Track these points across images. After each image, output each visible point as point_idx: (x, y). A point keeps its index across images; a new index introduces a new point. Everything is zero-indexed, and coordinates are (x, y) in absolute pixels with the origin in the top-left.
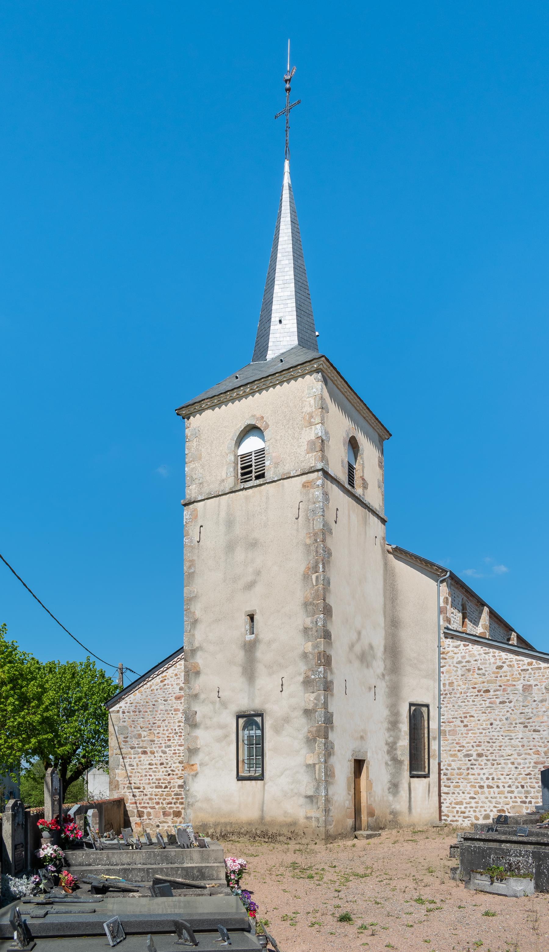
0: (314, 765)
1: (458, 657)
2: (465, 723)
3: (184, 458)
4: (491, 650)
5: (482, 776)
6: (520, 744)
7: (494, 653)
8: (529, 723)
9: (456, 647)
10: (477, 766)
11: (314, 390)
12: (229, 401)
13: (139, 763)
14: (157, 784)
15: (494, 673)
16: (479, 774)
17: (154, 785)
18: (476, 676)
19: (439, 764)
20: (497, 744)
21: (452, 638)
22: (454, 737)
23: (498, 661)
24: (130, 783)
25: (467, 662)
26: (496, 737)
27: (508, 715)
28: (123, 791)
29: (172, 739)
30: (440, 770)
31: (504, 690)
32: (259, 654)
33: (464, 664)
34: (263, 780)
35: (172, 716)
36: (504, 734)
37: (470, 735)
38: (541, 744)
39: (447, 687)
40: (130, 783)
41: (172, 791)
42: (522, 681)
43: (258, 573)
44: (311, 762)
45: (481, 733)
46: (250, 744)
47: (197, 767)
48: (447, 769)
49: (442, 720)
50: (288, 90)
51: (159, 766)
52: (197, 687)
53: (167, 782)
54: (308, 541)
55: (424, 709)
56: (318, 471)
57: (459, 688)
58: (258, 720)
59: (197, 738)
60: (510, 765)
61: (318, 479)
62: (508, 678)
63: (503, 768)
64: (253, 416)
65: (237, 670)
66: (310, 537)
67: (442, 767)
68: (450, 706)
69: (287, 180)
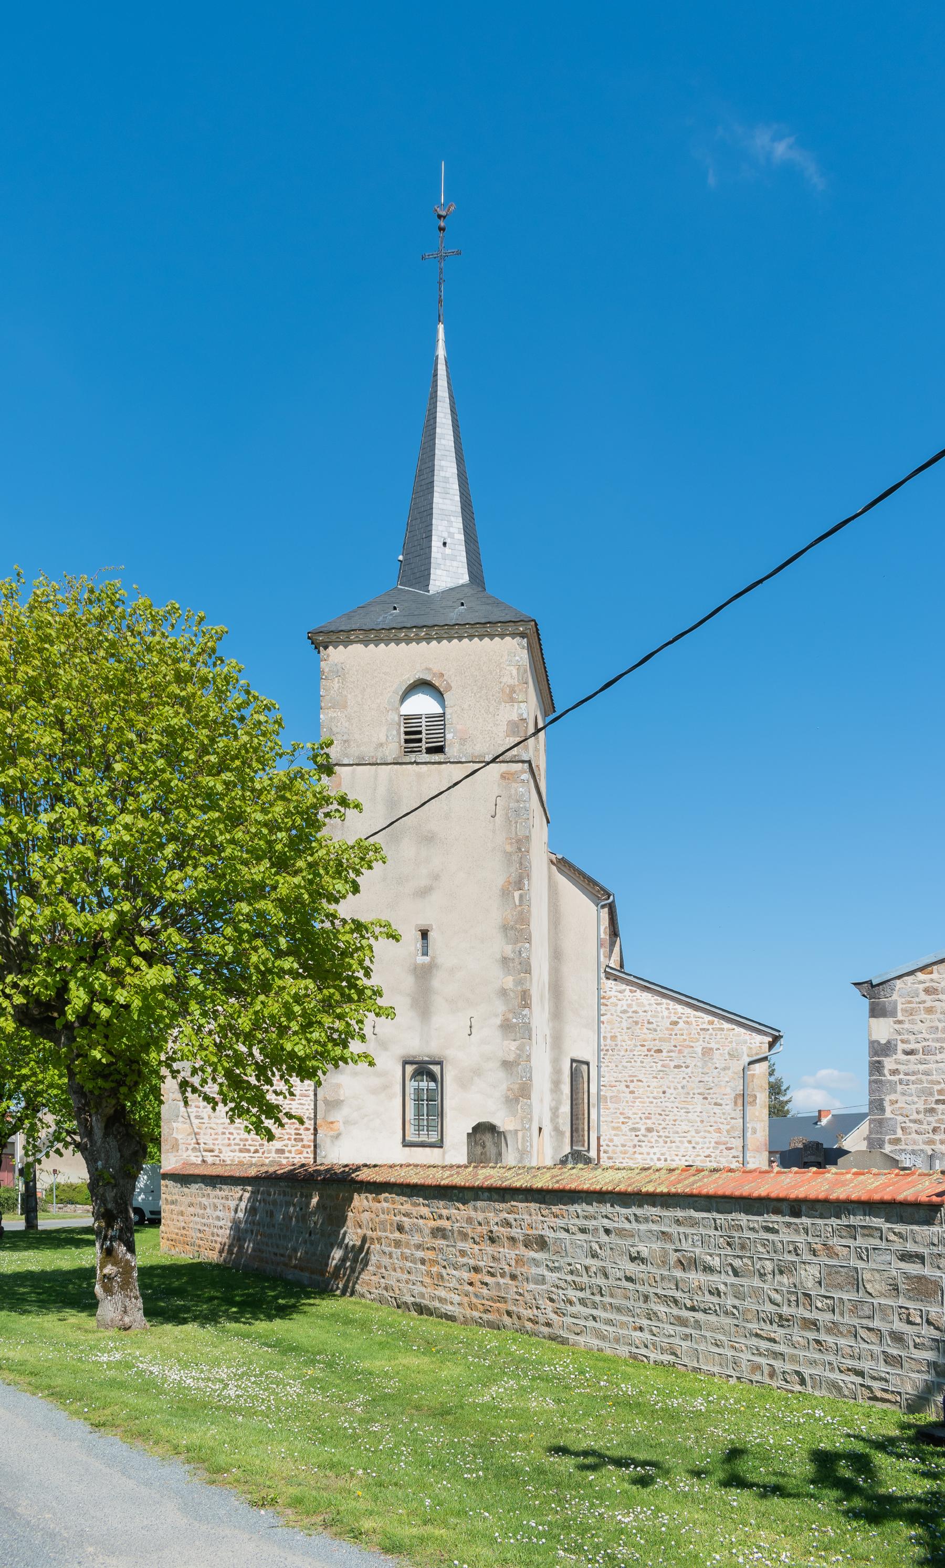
0: (516, 1131)
1: (623, 1005)
2: (632, 1089)
3: (319, 702)
4: (664, 1001)
5: (652, 1156)
6: (699, 1119)
7: (667, 1004)
8: (709, 1094)
9: (620, 992)
10: (646, 1143)
11: (517, 658)
12: (391, 640)
15: (667, 1029)
16: (648, 1154)
17: (237, 1147)
18: (645, 1031)
19: (599, 1138)
20: (671, 1117)
21: (615, 980)
22: (616, 1106)
23: (672, 1015)
24: (198, 1144)
25: (633, 1012)
26: (670, 1109)
27: (685, 1082)
28: (185, 1155)
30: (599, 1145)
31: (680, 1052)
32: (436, 983)
33: (630, 1014)
34: (442, 1147)
36: (679, 1106)
37: (637, 1104)
38: (722, 1120)
39: (608, 1041)
40: (198, 1144)
41: (266, 1158)
42: (701, 1042)
43: (436, 877)
45: (652, 1103)
46: (418, 1099)
47: (340, 1126)
48: (608, 1145)
49: (602, 1083)
50: (441, 229)
53: (257, 1144)
54: (509, 848)
55: (585, 1067)
56: (523, 762)
57: (624, 1044)
58: (436, 1069)
60: (686, 1144)
61: (523, 772)
62: (684, 1037)
63: (678, 1147)
64: (429, 669)
66: (511, 843)
67: (602, 1143)
68: (612, 1065)
69: (441, 352)
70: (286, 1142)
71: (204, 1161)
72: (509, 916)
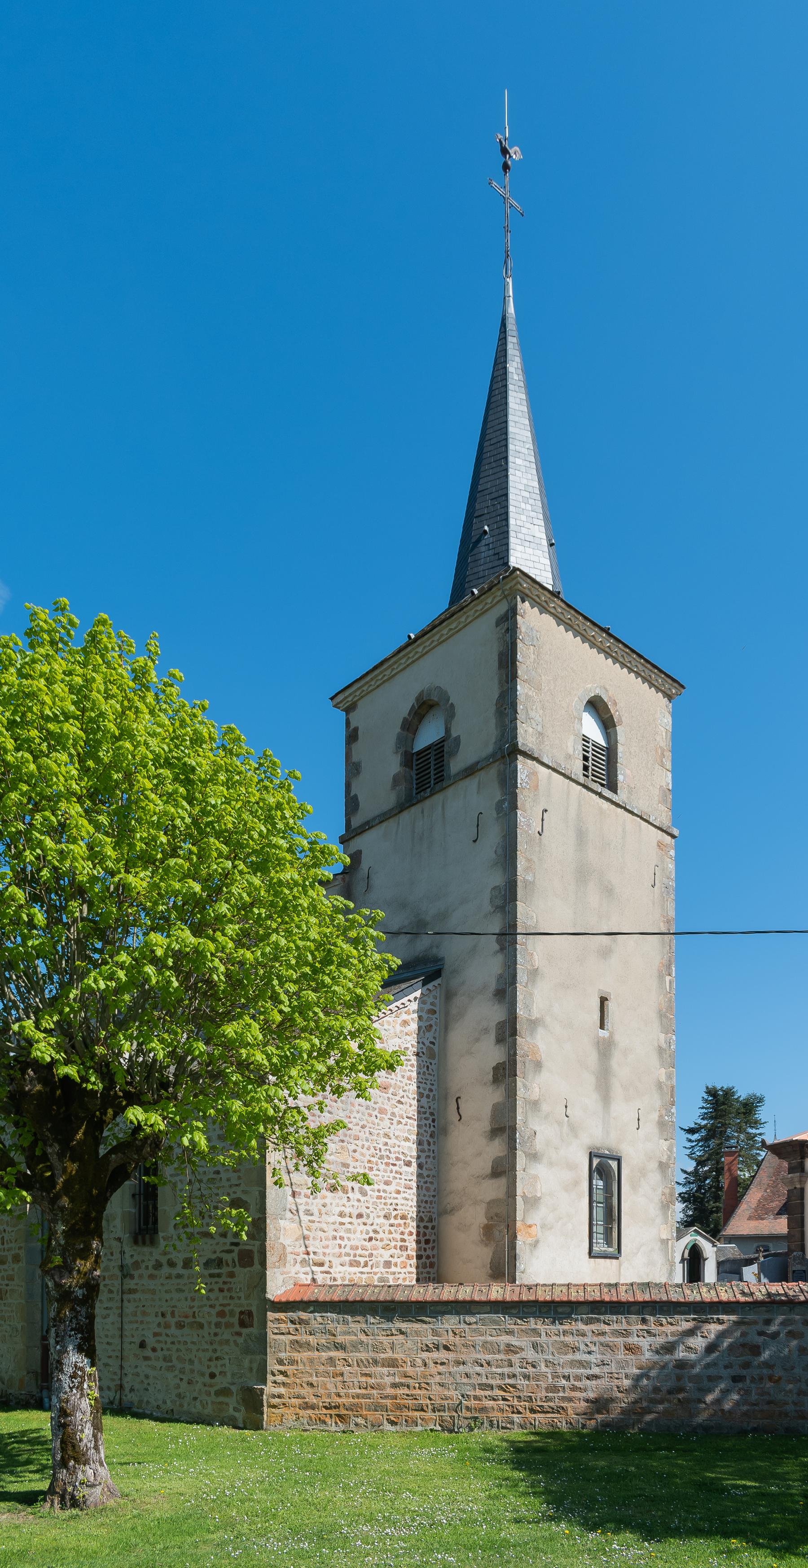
0: (668, 1240)
13: (324, 1210)
14: (352, 1258)
17: (347, 1259)
24: (308, 1253)
28: (293, 1270)
29: (375, 1167)
34: (617, 1258)
35: (377, 1121)
40: (308, 1253)
44: (664, 1237)
51: (354, 1220)
52: (537, 1090)
59: (535, 1178)
65: (590, 1080)
70: (393, 1251)
71: (314, 1280)
72: (128, 962)
